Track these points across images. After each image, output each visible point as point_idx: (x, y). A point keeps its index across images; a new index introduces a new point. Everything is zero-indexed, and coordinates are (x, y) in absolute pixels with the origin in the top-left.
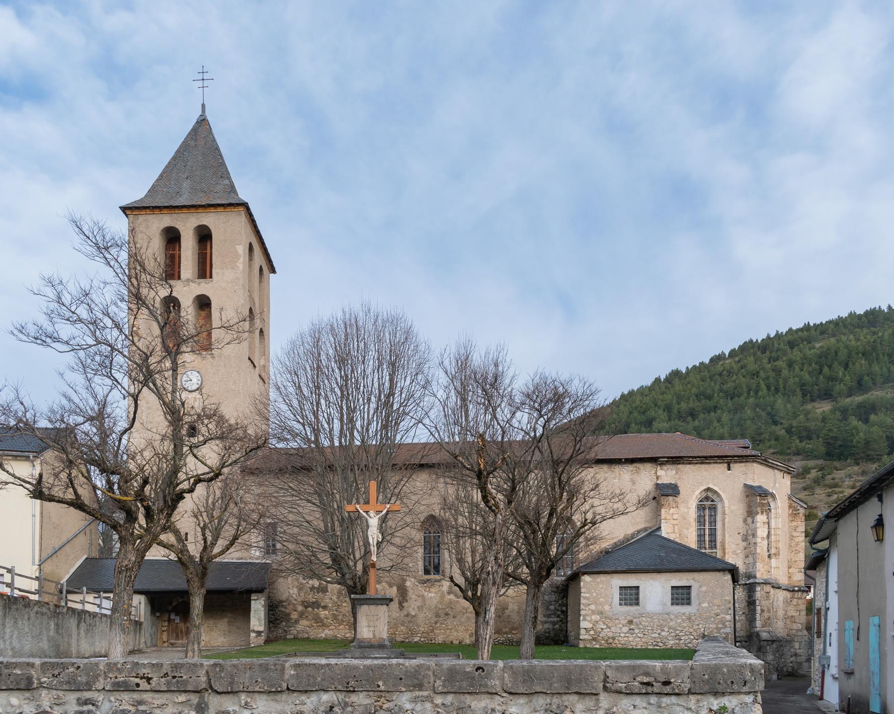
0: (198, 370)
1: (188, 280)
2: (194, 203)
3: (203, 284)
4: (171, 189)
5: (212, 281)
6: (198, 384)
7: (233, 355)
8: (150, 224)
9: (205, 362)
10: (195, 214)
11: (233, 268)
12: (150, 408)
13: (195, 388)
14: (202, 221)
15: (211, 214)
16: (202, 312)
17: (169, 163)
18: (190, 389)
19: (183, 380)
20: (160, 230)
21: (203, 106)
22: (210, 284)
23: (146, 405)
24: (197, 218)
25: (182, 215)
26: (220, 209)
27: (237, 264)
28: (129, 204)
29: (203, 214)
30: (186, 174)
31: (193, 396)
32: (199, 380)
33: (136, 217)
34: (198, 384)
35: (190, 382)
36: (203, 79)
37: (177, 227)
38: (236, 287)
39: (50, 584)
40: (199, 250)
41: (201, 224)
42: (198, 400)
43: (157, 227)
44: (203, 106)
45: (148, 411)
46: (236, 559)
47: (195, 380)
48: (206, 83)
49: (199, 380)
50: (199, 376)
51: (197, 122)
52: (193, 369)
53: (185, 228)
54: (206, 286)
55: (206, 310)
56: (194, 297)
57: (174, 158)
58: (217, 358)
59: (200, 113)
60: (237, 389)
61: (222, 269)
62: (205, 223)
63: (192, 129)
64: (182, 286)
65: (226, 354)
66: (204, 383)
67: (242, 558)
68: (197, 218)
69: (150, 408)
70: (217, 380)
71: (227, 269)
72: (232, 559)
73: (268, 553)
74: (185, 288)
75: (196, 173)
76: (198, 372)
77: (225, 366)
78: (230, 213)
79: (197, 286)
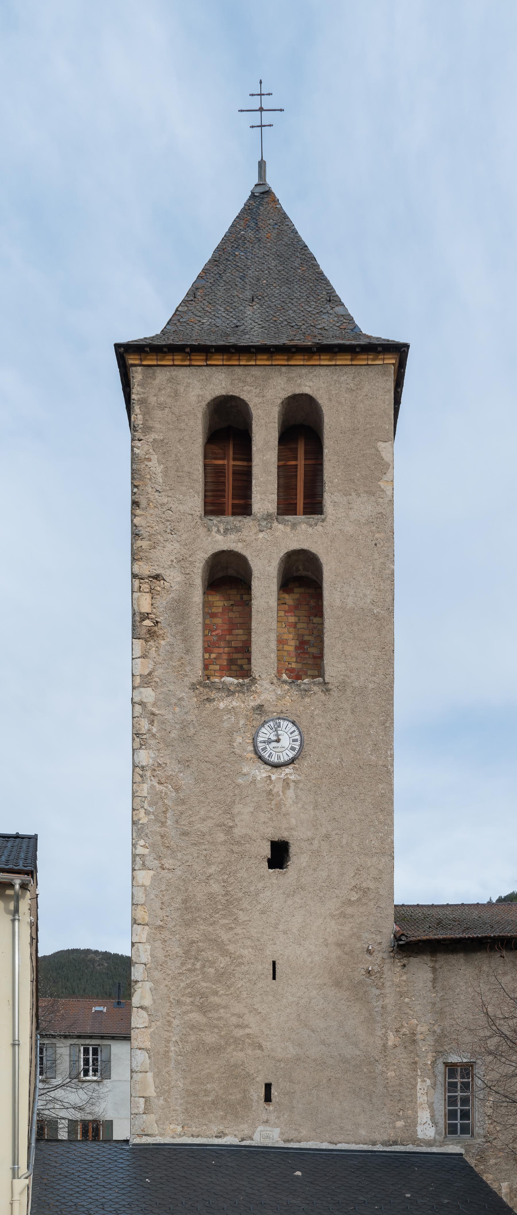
0: (294, 718)
1: (268, 517)
2: (283, 340)
3: (304, 526)
4: (218, 320)
5: (323, 521)
6: (293, 749)
7: (371, 686)
8: (181, 389)
9: (307, 700)
10: (284, 369)
11: (371, 493)
12: (183, 802)
13: (287, 759)
14: (300, 385)
15: (322, 371)
16: (286, 596)
17: (205, 271)
18: (274, 759)
19: (260, 739)
20: (204, 404)
21: (262, 165)
22: (319, 528)
23: (174, 794)
24: (289, 380)
25: (255, 371)
26: (343, 360)
27: (381, 483)
28: (136, 341)
29: (304, 371)
30: (248, 294)
31: (282, 776)
32: (294, 741)
33: (150, 371)
34: (293, 749)
35: (274, 744)
36: (261, 109)
37: (244, 396)
38: (377, 535)
39: (63, 1121)
40: (279, 460)
41: (298, 391)
42: (292, 785)
43: (199, 396)
44: (262, 165)
45: (180, 808)
46: (384, 1144)
47: (286, 741)
48: (267, 118)
49: (294, 741)
50: (297, 733)
51: (253, 196)
52: (282, 716)
53: (260, 400)
54: (310, 530)
55: (296, 590)
56: (282, 554)
57: (214, 261)
58: (335, 693)
59: (256, 181)
60: (381, 763)
61: (347, 494)
62: (307, 390)
63: (244, 208)
64: (255, 529)
65: (356, 684)
66: (306, 748)
67: (395, 1143)
68: (289, 380)
69: (183, 802)
70: (336, 741)
71: (359, 495)
72: (374, 1144)
73: (452, 1130)
74: (261, 535)
75: (269, 291)
76: (293, 723)
77: (353, 712)
78: (363, 370)
79: (288, 529)
